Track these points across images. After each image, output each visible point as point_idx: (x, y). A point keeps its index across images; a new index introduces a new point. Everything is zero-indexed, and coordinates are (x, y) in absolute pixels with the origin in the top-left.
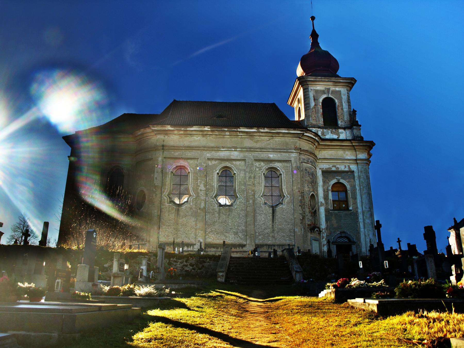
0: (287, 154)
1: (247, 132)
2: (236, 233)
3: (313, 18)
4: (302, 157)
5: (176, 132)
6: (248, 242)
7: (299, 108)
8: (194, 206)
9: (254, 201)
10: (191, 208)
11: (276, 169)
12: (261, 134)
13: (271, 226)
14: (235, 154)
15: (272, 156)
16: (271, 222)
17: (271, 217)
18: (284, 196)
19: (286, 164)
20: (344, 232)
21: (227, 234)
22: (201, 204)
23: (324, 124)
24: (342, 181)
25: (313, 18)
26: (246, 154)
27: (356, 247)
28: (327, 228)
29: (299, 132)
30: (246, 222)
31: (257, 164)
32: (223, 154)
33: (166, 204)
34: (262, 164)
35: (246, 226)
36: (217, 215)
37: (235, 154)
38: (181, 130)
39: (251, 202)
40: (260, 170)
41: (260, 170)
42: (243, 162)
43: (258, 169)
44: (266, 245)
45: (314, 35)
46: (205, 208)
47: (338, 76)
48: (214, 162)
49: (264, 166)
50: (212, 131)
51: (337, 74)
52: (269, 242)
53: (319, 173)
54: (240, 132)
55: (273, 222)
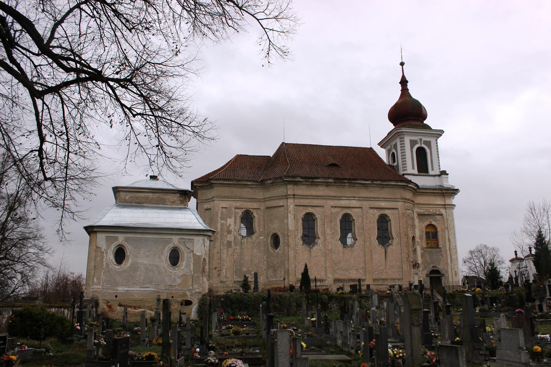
0: (395, 203)
1: (363, 184)
2: (357, 270)
3: (402, 64)
4: (407, 204)
5: (304, 183)
6: (367, 277)
7: (393, 154)
8: (323, 248)
9: (370, 243)
10: (320, 250)
11: (386, 215)
12: (374, 186)
13: (384, 264)
14: (354, 203)
15: (383, 204)
16: (384, 260)
17: (384, 256)
18: (393, 238)
19: (394, 211)
20: (436, 267)
21: (350, 271)
22: (328, 246)
23: (419, 171)
24: (433, 223)
25: (402, 64)
26: (363, 202)
27: (31, 181)
28: (422, 263)
29: (405, 184)
30: (365, 261)
31: (371, 211)
32: (344, 203)
33: (300, 246)
34: (375, 211)
35: (365, 264)
36: (342, 255)
37: (354, 203)
38: (309, 181)
39: (368, 244)
40: (374, 216)
41: (374, 216)
42: (360, 209)
43: (372, 216)
44: (381, 279)
45: (404, 82)
46: (331, 249)
47: (427, 127)
48: (336, 210)
49: (377, 213)
50: (334, 182)
51: (425, 122)
52: (383, 277)
53: (416, 215)
54: (357, 183)
55: (386, 260)
